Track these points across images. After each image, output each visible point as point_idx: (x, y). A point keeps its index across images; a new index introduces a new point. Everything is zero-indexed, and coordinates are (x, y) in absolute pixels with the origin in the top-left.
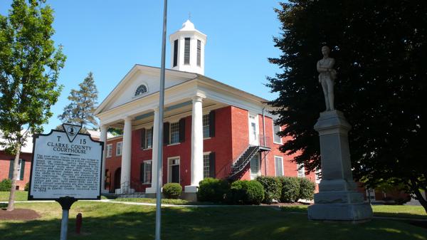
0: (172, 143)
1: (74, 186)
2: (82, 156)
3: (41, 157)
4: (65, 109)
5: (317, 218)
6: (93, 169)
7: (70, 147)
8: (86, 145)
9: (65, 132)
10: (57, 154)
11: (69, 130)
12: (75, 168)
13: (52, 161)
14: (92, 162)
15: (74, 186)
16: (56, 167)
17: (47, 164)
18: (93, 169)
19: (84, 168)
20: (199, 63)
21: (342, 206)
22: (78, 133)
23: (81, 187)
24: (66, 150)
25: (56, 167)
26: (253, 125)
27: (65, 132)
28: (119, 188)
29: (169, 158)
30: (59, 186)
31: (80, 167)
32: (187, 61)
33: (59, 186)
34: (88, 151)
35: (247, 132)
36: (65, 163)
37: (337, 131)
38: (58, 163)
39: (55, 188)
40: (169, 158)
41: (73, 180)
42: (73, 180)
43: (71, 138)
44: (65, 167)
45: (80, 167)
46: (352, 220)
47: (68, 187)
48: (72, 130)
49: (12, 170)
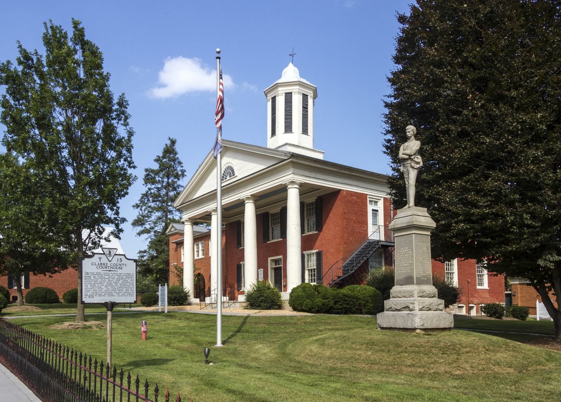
0: (273, 239)
1: (115, 294)
2: (120, 271)
3: (88, 273)
4: (127, 193)
5: (402, 327)
6: (129, 281)
7: (109, 265)
8: (122, 263)
9: (104, 254)
10: (100, 271)
11: (108, 253)
12: (115, 280)
13: (97, 276)
14: (128, 275)
15: (115, 294)
16: (100, 280)
17: (92, 278)
18: (129, 281)
19: (122, 280)
20: (305, 131)
21: (408, 314)
22: (115, 254)
23: (121, 294)
24: (106, 268)
25: (100, 280)
26: (375, 211)
27: (104, 254)
28: (209, 295)
29: (269, 259)
30: (103, 294)
31: (118, 280)
32: (288, 128)
33: (103, 294)
34: (124, 267)
35: (365, 223)
36: (106, 277)
37: (429, 233)
38: (101, 278)
39: (100, 295)
40: (269, 259)
41: (114, 290)
42: (114, 290)
43: (110, 259)
44: (107, 280)
45: (118, 280)
46: (415, 329)
47: (111, 295)
48: (110, 253)
49: (111, 360)
